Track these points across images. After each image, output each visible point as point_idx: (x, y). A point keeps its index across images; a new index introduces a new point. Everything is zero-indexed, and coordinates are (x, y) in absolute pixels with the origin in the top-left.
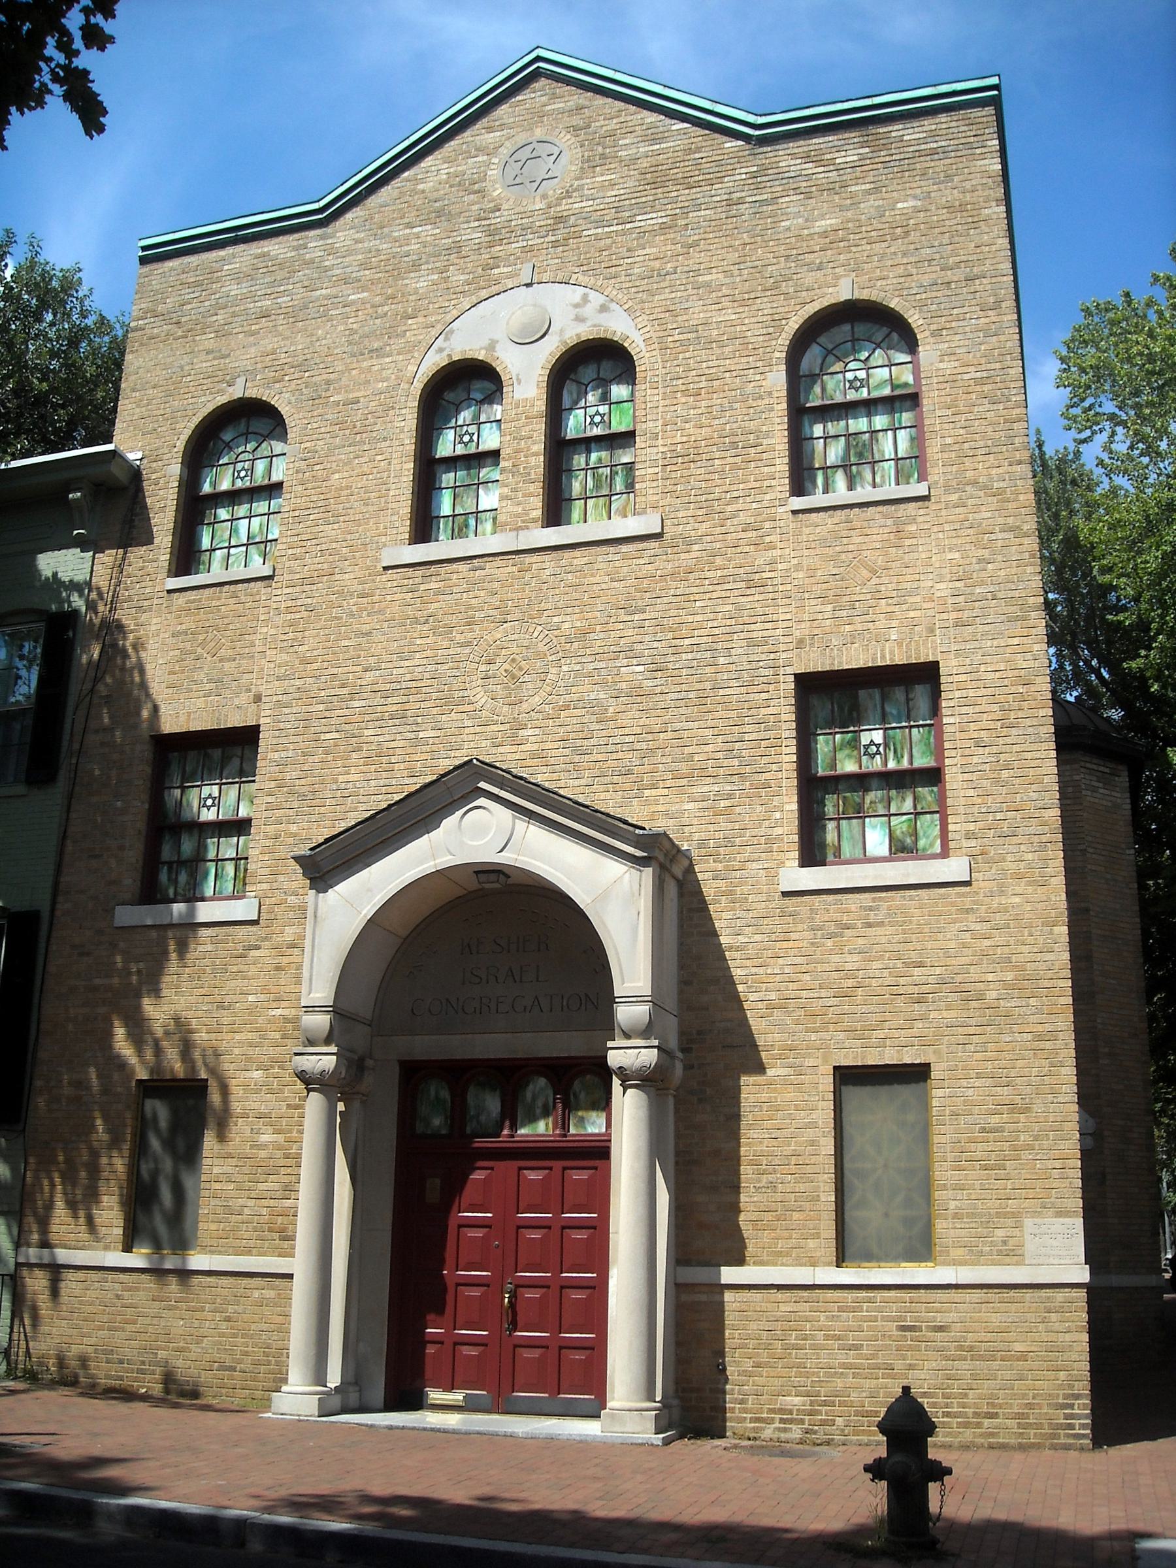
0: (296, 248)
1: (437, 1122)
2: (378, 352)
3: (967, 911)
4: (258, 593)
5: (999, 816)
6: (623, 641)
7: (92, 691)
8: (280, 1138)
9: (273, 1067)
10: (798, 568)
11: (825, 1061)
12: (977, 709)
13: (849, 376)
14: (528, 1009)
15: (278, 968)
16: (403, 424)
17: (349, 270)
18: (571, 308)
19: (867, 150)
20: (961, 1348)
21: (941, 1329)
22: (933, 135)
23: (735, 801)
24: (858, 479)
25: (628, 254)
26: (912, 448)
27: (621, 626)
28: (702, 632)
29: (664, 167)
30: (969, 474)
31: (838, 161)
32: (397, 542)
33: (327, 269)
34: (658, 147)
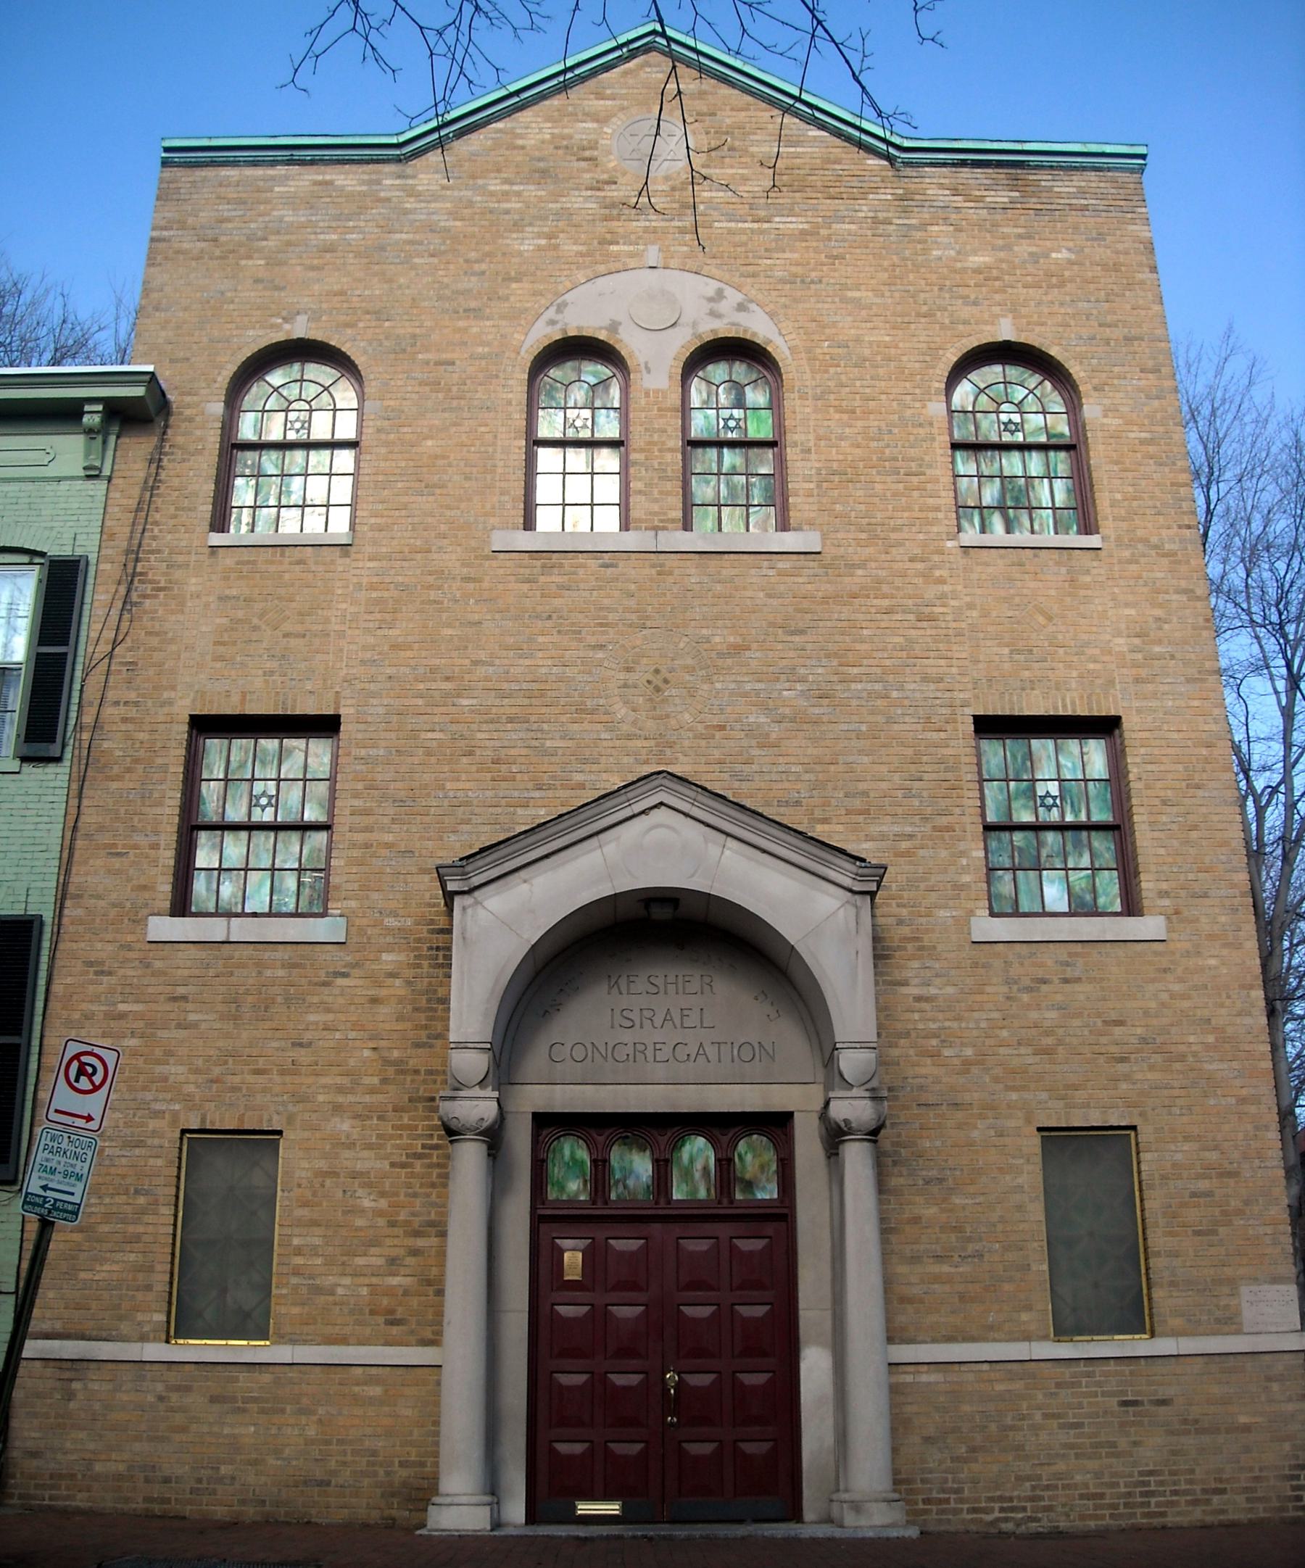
0: (370, 183)
1: (574, 1186)
2: (476, 313)
3: (1165, 971)
4: (333, 562)
5: (1191, 876)
6: (784, 662)
7: (111, 655)
8: (383, 1203)
9: (370, 1118)
10: (971, 606)
11: (1028, 1121)
12: (1162, 767)
13: (1004, 417)
14: (692, 1058)
15: (375, 1001)
16: (510, 396)
17: (435, 217)
18: (705, 302)
19: (1017, 194)
20: (1185, 1421)
21: (1163, 1402)
22: (1082, 193)
23: (917, 842)
24: (1015, 524)
25: (767, 254)
26: (1069, 500)
27: (780, 646)
28: (871, 662)
29: (802, 172)
30: (1140, 533)
31: (988, 199)
32: (505, 527)
33: (407, 212)
34: (792, 150)
